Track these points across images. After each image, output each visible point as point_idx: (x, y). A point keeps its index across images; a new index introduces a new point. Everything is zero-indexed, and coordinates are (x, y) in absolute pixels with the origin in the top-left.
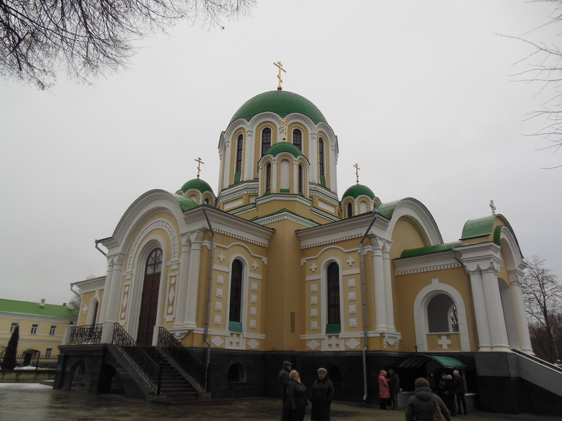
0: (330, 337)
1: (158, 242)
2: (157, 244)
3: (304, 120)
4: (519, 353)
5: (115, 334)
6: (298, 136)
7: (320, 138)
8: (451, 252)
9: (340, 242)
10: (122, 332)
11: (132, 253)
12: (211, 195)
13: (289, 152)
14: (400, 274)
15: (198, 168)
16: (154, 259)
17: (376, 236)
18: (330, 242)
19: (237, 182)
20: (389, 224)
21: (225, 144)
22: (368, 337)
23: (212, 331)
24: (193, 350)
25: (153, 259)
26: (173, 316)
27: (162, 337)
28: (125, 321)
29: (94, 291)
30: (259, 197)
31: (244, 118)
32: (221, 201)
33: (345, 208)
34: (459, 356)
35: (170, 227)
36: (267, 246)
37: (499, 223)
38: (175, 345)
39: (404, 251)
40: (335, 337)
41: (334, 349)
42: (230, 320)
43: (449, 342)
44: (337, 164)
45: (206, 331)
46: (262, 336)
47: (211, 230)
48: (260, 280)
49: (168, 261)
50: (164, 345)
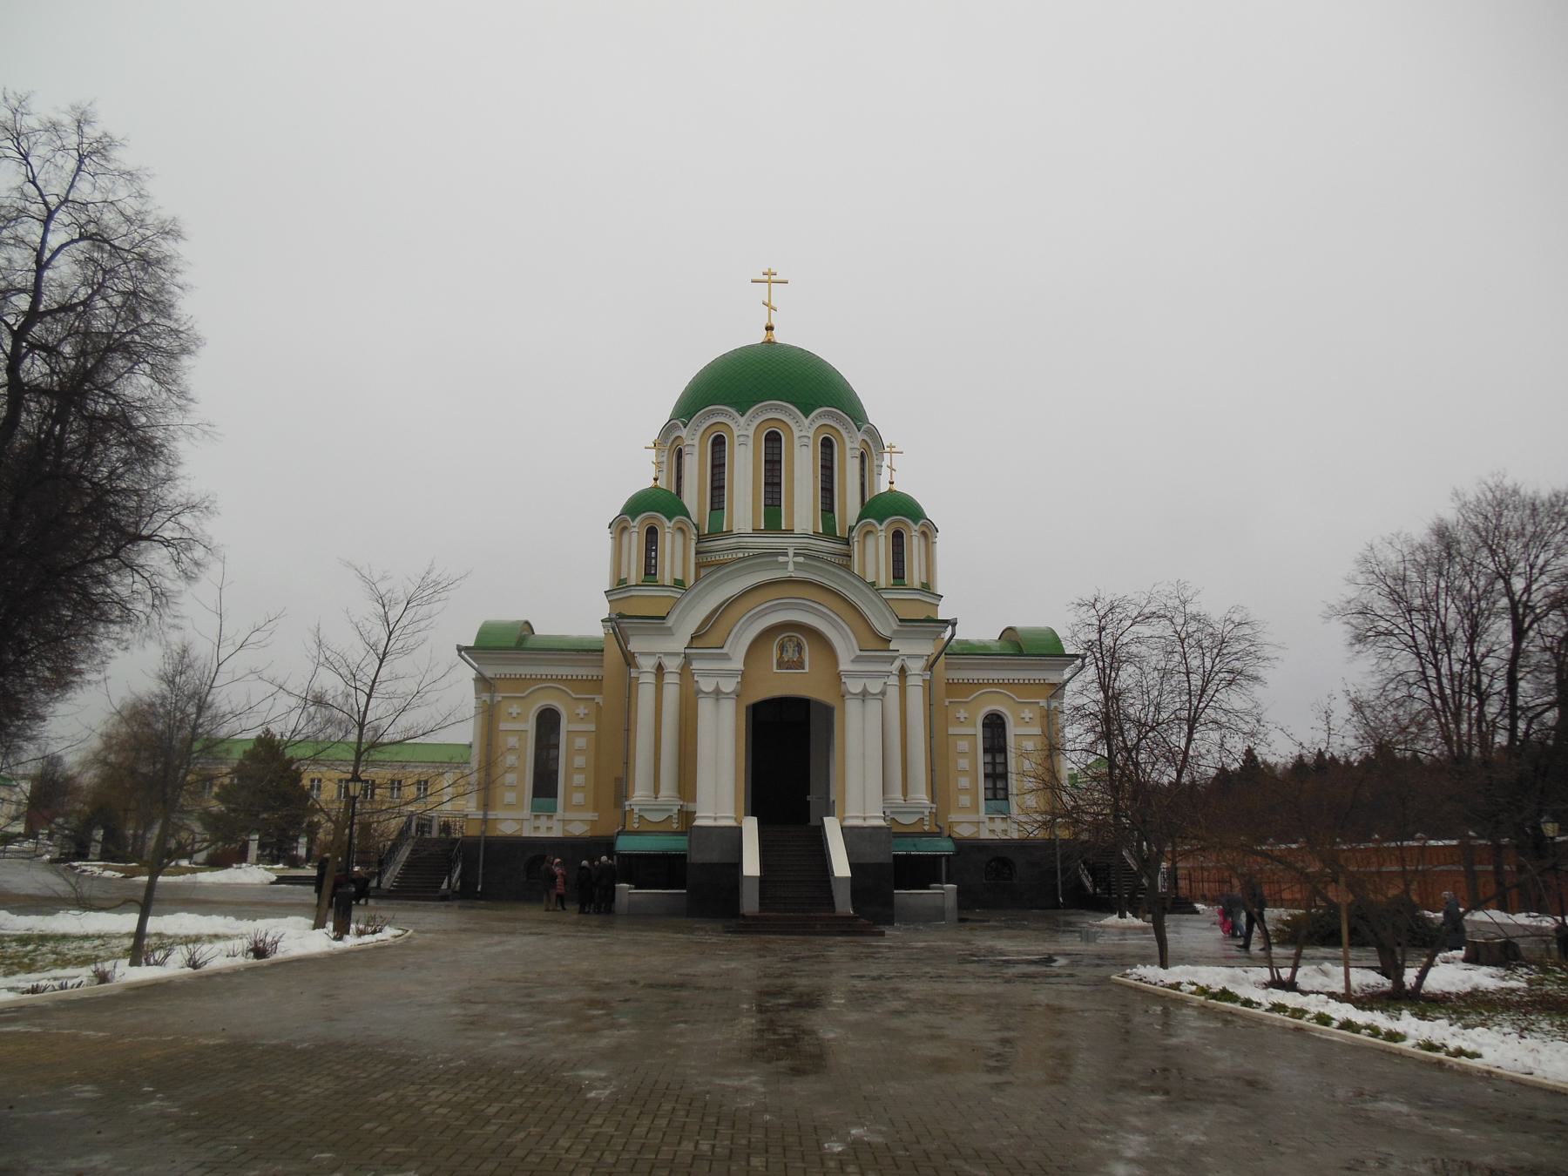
0: (537, 817)
6: (828, 451)
40: (545, 818)
46: (591, 816)
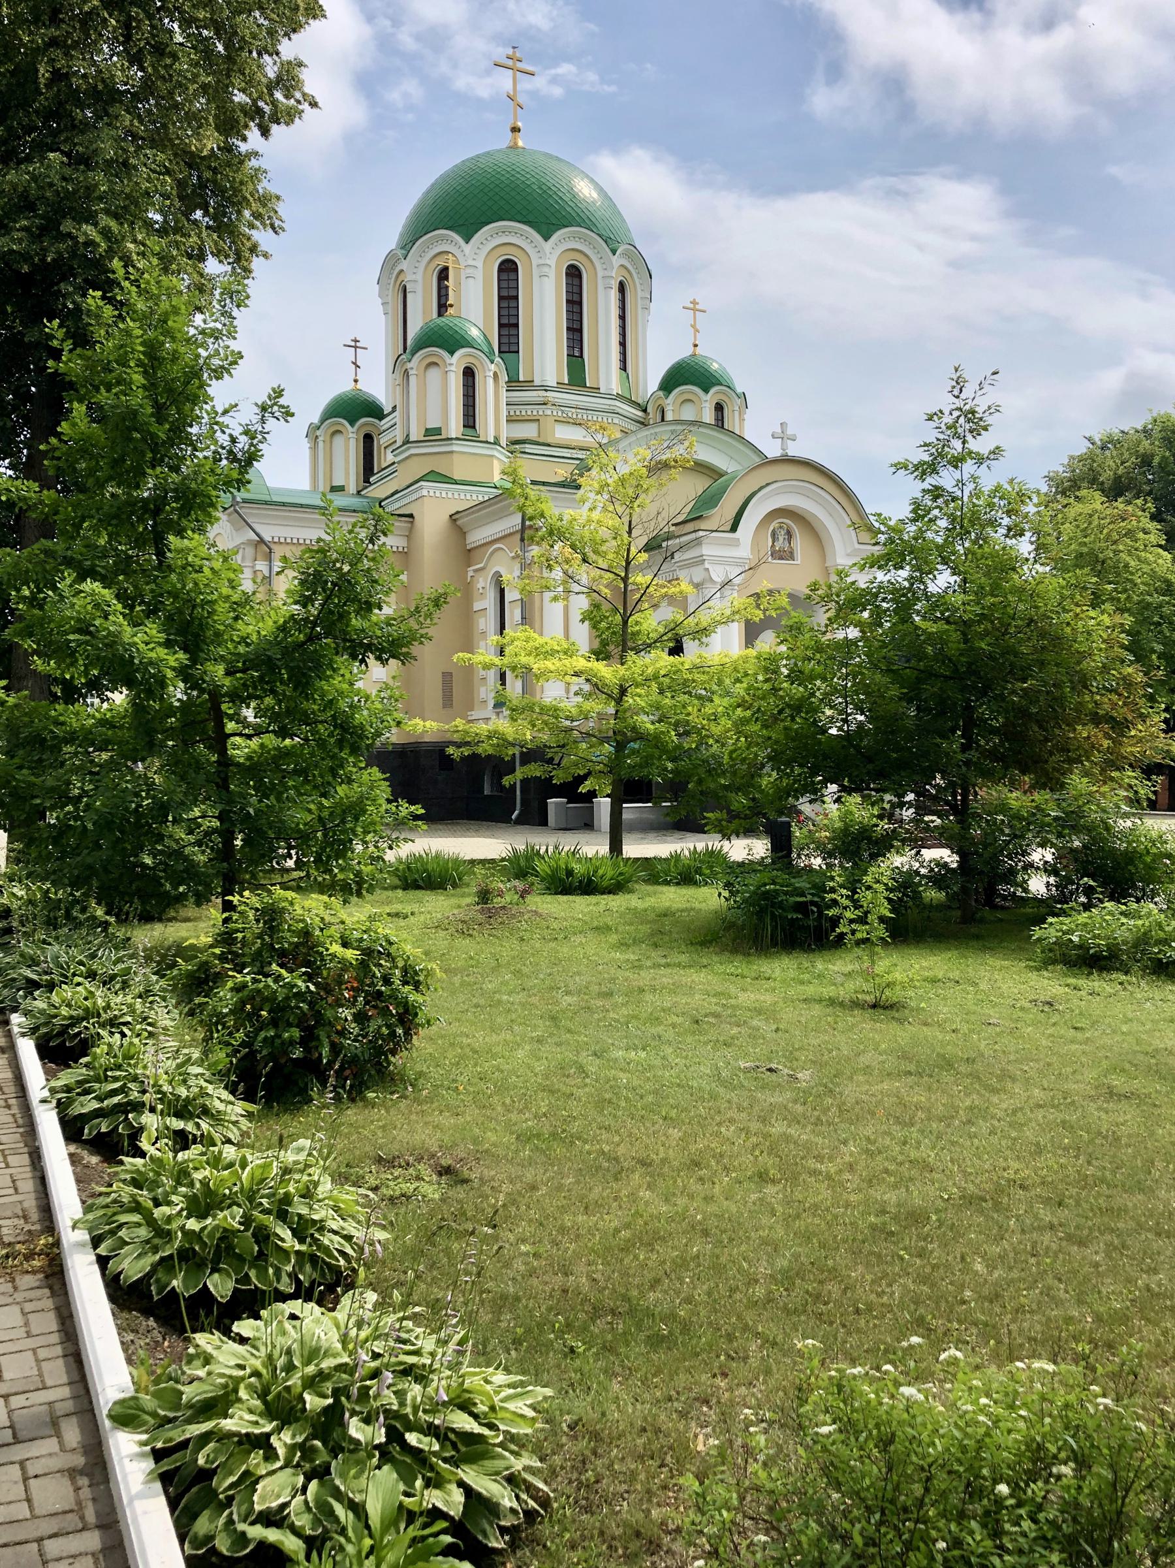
6: (576, 281)
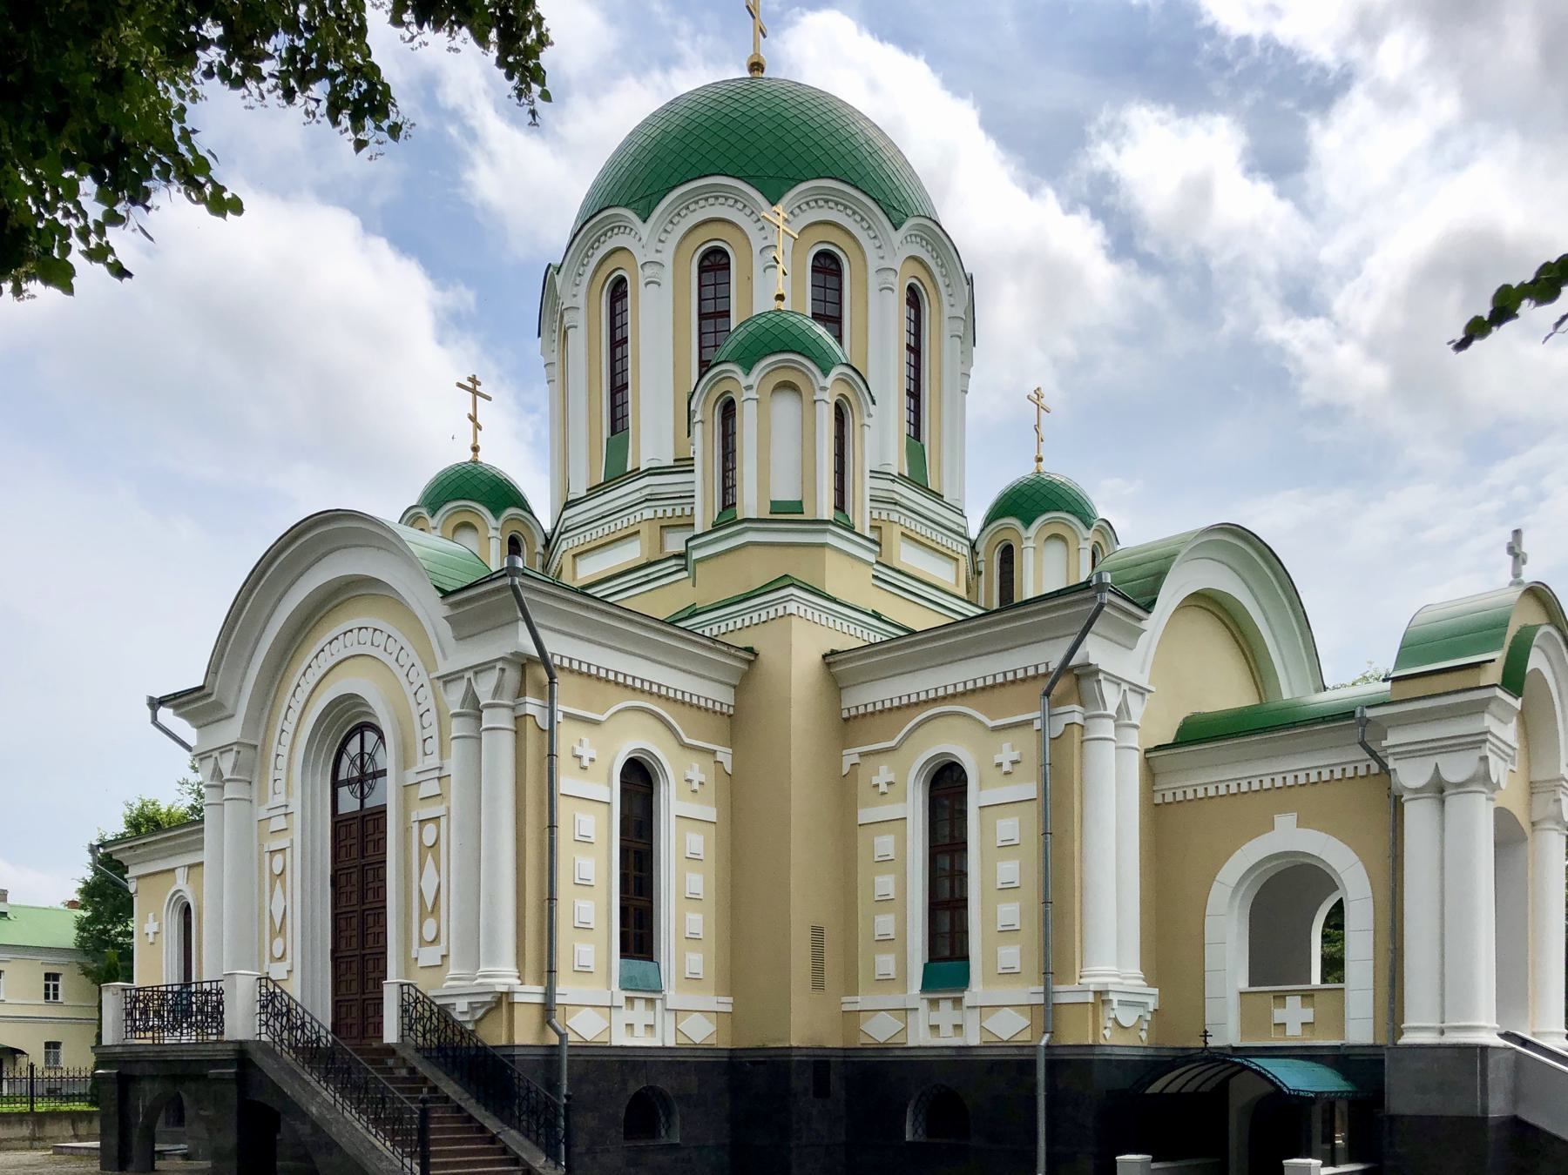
0: (934, 1003)
1: (366, 704)
2: (364, 709)
3: (854, 213)
4: (1525, 1042)
5: (267, 1012)
6: (831, 281)
7: (912, 289)
8: (1354, 721)
9: (973, 691)
10: (287, 1006)
11: (280, 743)
12: (528, 527)
13: (799, 353)
14: (1169, 798)
15: (470, 417)
16: (358, 763)
17: (1098, 671)
18: (941, 693)
19: (617, 474)
20: (1144, 625)
21: (562, 316)
22: (1054, 1004)
23: (566, 991)
24: (514, 1056)
25: (352, 761)
26: (440, 949)
27: (414, 1016)
28: (285, 966)
29: (173, 870)
30: (698, 530)
31: (626, 206)
32: (564, 546)
33: (989, 563)
34: (1341, 1059)
35: (402, 648)
36: (731, 711)
37: (1532, 615)
38: (457, 1039)
39: (1187, 717)
40: (949, 1004)
41: (948, 1039)
42: (622, 957)
43: (1308, 1015)
44: (966, 392)
45: (549, 993)
46: (725, 1004)
47: (544, 659)
48: (713, 826)
49: (405, 769)
50: (420, 1040)
